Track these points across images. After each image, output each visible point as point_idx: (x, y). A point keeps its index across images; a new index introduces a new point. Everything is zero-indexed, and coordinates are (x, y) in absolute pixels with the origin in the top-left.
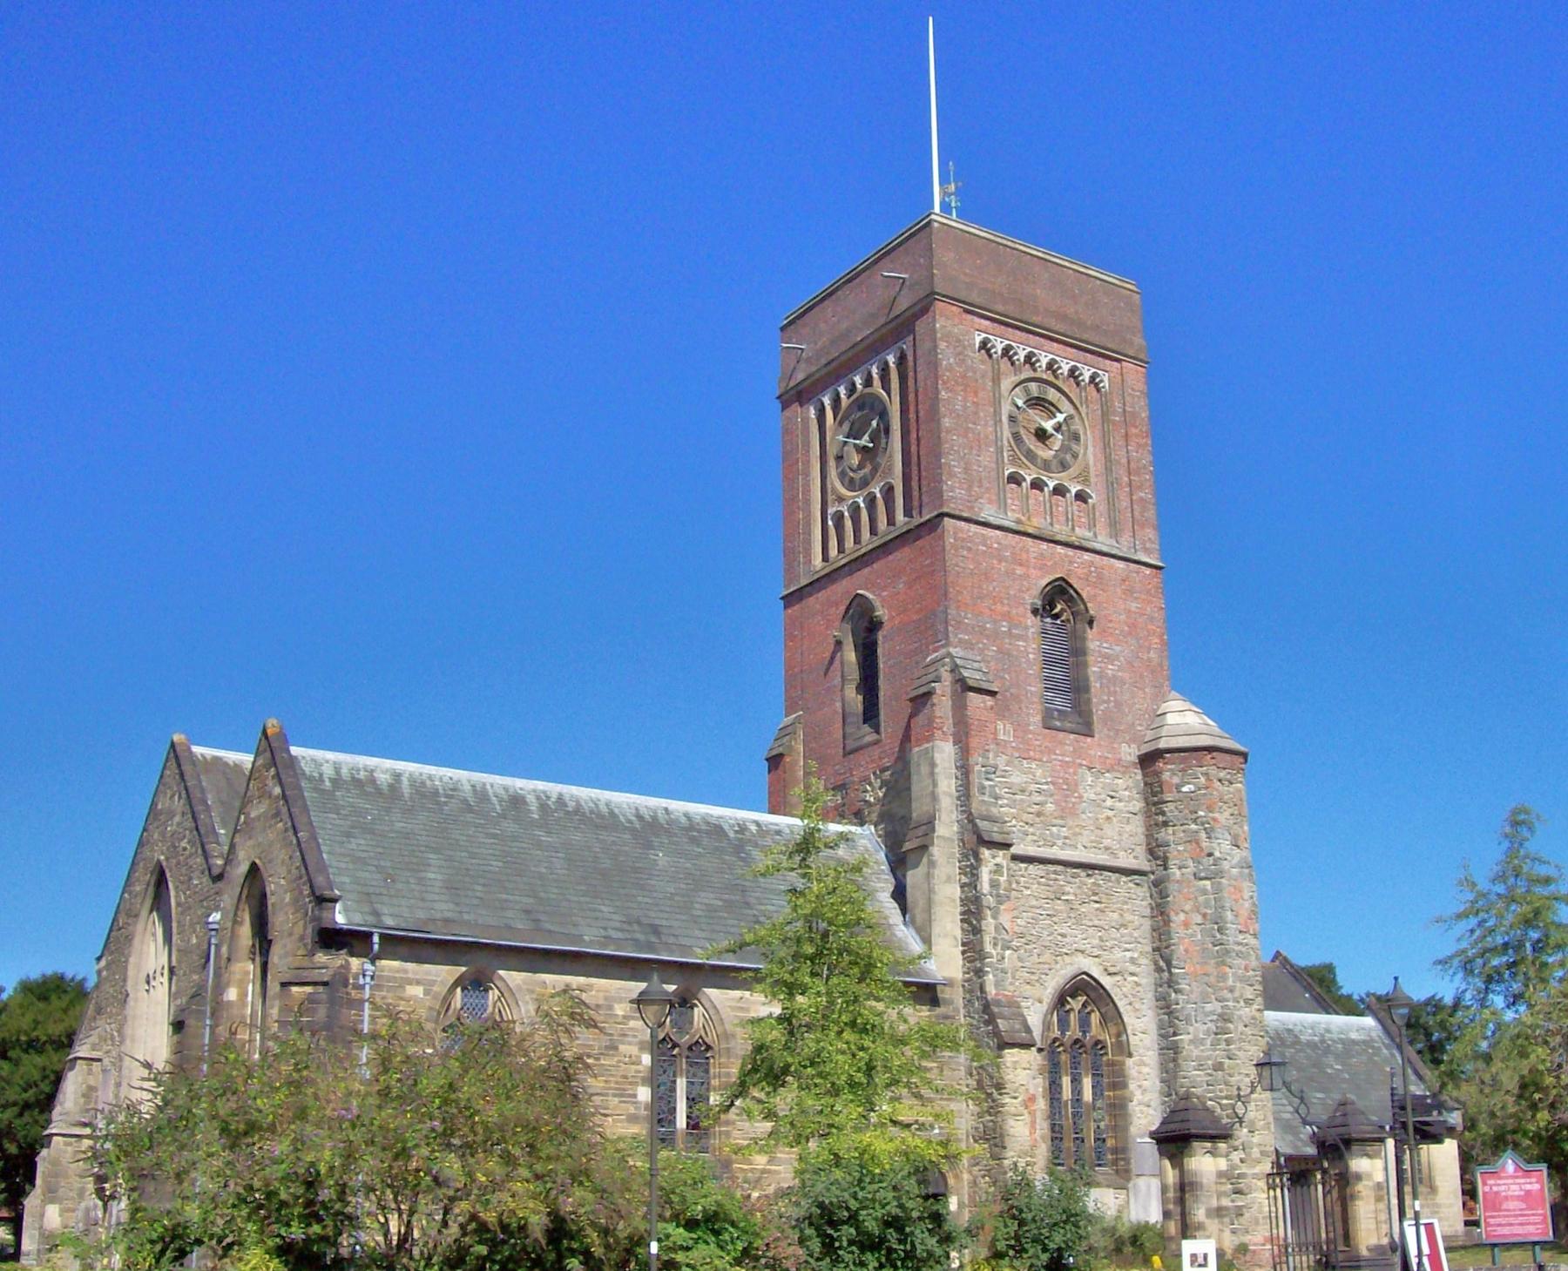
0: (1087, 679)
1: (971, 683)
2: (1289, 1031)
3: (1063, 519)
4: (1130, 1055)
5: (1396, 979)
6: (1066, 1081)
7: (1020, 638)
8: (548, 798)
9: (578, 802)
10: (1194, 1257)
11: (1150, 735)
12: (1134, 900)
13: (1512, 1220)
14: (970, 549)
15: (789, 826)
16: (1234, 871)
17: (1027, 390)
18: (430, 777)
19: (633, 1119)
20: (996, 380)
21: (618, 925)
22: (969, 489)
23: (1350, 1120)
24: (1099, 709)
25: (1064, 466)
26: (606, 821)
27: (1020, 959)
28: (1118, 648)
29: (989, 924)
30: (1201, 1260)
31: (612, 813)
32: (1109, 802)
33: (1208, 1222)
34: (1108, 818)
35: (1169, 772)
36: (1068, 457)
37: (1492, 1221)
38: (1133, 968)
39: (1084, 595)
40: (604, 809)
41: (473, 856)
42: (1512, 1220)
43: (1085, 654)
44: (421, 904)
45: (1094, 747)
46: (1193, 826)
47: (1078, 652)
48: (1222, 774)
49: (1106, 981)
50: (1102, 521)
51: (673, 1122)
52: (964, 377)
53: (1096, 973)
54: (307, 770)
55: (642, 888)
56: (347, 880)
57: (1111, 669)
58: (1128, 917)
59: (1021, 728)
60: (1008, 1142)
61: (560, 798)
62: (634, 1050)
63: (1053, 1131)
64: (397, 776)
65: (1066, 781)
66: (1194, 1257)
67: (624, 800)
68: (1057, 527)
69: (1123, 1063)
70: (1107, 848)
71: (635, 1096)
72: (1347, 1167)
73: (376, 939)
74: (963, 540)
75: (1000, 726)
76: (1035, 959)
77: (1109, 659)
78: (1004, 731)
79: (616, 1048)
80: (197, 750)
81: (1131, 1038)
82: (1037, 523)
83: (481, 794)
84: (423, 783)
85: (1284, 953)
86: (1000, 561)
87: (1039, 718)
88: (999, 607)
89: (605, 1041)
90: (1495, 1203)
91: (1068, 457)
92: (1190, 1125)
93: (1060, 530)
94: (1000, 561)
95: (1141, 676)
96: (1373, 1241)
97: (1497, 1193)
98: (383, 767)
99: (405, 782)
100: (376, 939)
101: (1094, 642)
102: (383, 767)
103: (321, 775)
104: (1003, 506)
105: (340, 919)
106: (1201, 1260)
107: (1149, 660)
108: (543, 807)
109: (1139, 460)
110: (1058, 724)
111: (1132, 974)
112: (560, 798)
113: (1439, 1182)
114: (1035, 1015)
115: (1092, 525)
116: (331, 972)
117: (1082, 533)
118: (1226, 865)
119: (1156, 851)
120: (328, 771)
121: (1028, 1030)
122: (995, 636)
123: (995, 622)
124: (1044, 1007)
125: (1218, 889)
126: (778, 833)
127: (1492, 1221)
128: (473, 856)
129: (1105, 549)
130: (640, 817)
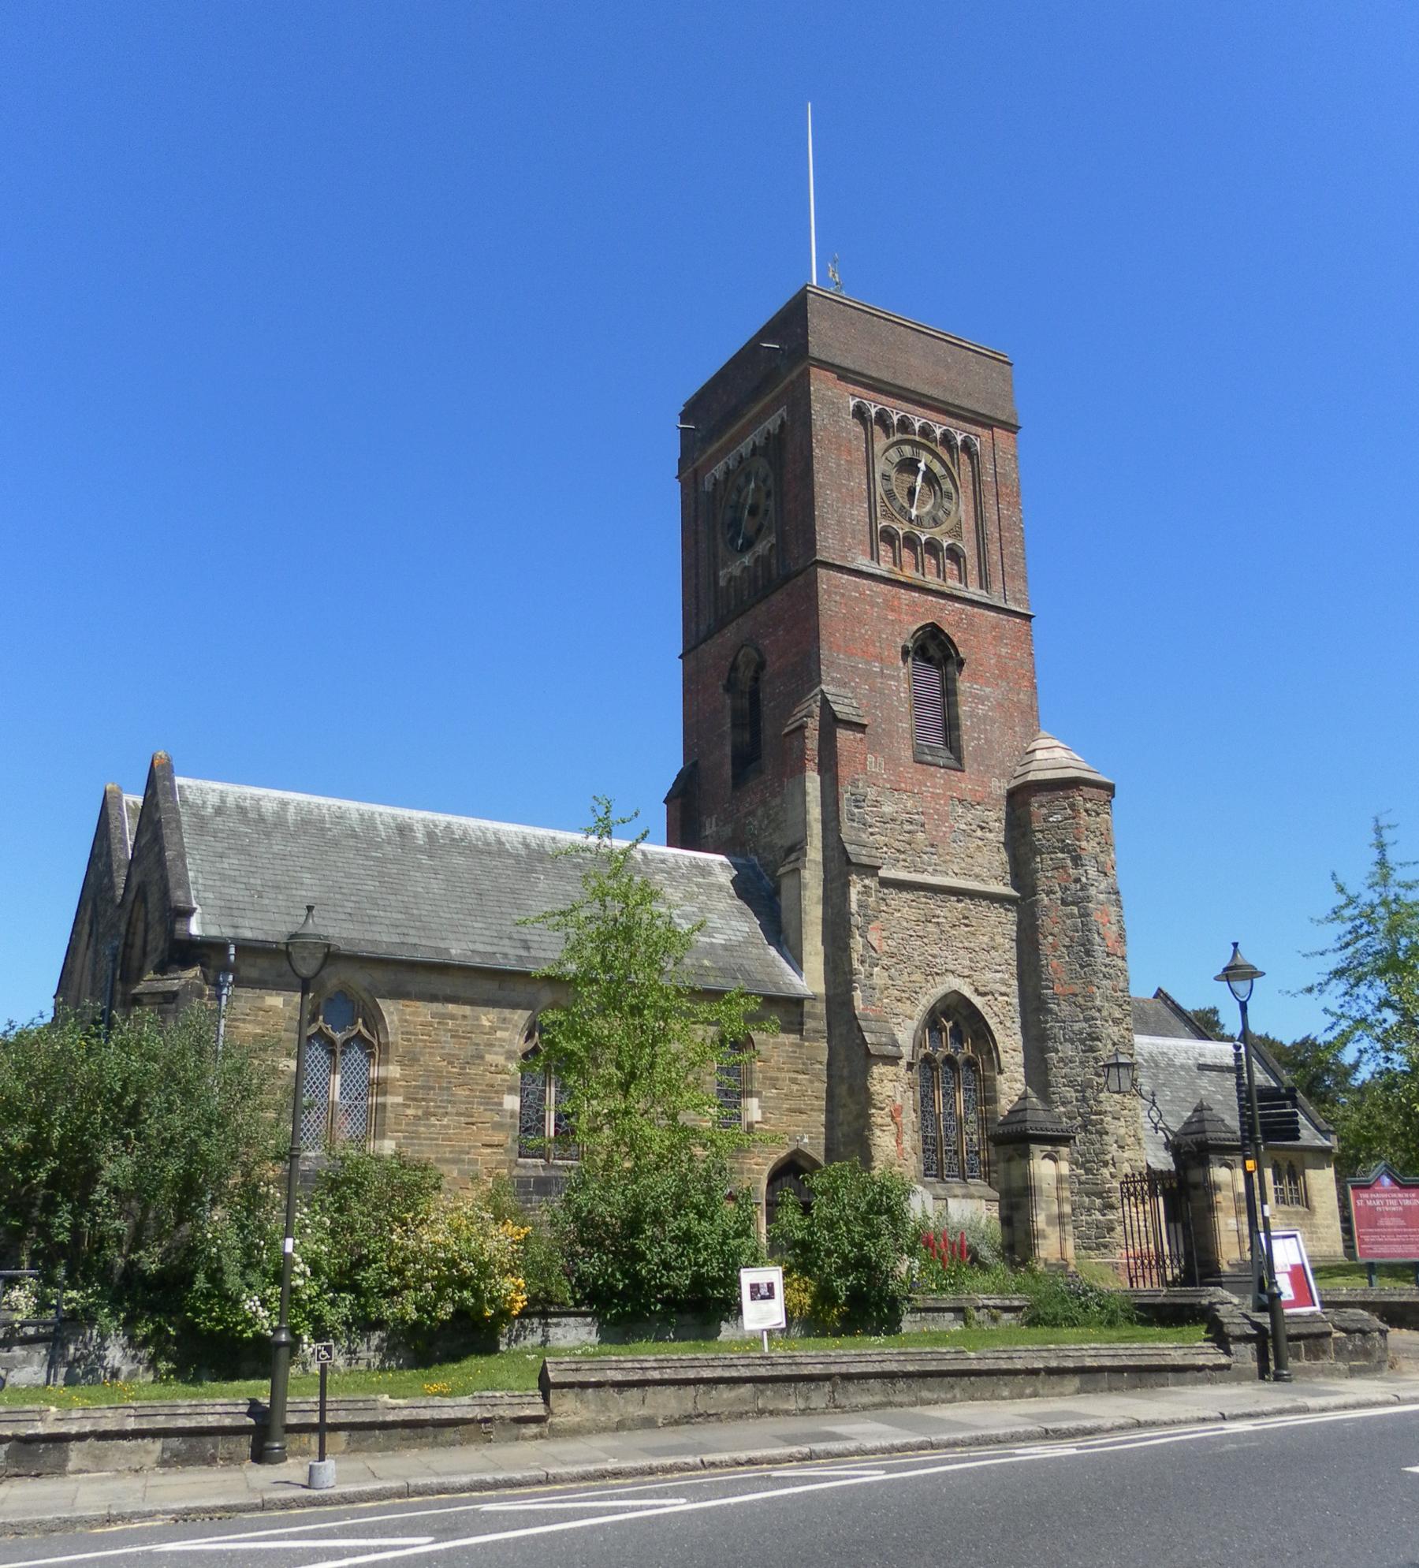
0: (957, 718)
1: (840, 716)
2: (1163, 1053)
3: (934, 571)
4: (1001, 1072)
5: (1235, 945)
6: (939, 1095)
7: (892, 677)
8: (436, 826)
9: (465, 832)
10: (755, 1288)
11: (1020, 770)
12: (1001, 926)
13: (1389, 1239)
14: (843, 595)
15: (674, 856)
16: (1102, 897)
17: (900, 452)
18: (318, 807)
19: (498, 1126)
20: (869, 442)
21: (490, 940)
22: (843, 539)
23: (1207, 1126)
24: (969, 745)
25: (936, 522)
26: (496, 850)
27: (891, 978)
28: (988, 690)
29: (857, 943)
31: (500, 842)
32: (979, 833)
33: (1049, 1230)
34: (979, 847)
35: (1038, 807)
36: (941, 513)
37: (1366, 1238)
38: (1004, 989)
39: (955, 640)
40: (491, 838)
41: (348, 875)
42: (1389, 1239)
43: (955, 694)
44: (287, 918)
45: (965, 783)
46: (1060, 855)
47: (949, 693)
48: (1089, 805)
49: (978, 1001)
50: (973, 574)
51: (541, 1131)
52: (838, 437)
53: (967, 992)
54: (191, 798)
56: (211, 895)
57: (981, 710)
58: (999, 940)
59: (892, 761)
60: (875, 1152)
61: (448, 827)
62: (501, 1060)
63: (925, 1143)
64: (284, 804)
65: (937, 811)
66: (755, 1288)
68: (928, 578)
69: (995, 1079)
70: (977, 876)
71: (501, 1104)
72: (1206, 1174)
73: (232, 950)
74: (836, 587)
75: (871, 758)
76: (906, 977)
77: (981, 700)
78: (874, 763)
79: (482, 1058)
81: (1003, 1056)
82: (909, 573)
83: (369, 823)
84: (310, 812)
85: (1165, 990)
86: (872, 607)
87: (909, 753)
88: (871, 649)
89: (470, 1050)
90: (1372, 1218)
91: (941, 513)
92: (1028, 1125)
93: (932, 581)
94: (872, 607)
95: (1011, 715)
96: (1234, 1256)
97: (1374, 1207)
98: (269, 797)
99: (291, 809)
100: (232, 950)
101: (963, 684)
103: (204, 803)
104: (874, 556)
106: (764, 1291)
107: (1019, 701)
108: (431, 835)
109: (1010, 517)
110: (929, 758)
111: (1002, 994)
112: (448, 827)
113: (1316, 1201)
114: (906, 1033)
115: (962, 577)
116: (183, 982)
117: (953, 584)
118: (1093, 891)
119: (1021, 871)
121: (895, 1044)
122: (868, 675)
123: (867, 662)
124: (914, 1024)
125: (1084, 914)
126: (663, 861)
127: (1366, 1238)
128: (348, 875)
129: (975, 598)
130: (527, 846)
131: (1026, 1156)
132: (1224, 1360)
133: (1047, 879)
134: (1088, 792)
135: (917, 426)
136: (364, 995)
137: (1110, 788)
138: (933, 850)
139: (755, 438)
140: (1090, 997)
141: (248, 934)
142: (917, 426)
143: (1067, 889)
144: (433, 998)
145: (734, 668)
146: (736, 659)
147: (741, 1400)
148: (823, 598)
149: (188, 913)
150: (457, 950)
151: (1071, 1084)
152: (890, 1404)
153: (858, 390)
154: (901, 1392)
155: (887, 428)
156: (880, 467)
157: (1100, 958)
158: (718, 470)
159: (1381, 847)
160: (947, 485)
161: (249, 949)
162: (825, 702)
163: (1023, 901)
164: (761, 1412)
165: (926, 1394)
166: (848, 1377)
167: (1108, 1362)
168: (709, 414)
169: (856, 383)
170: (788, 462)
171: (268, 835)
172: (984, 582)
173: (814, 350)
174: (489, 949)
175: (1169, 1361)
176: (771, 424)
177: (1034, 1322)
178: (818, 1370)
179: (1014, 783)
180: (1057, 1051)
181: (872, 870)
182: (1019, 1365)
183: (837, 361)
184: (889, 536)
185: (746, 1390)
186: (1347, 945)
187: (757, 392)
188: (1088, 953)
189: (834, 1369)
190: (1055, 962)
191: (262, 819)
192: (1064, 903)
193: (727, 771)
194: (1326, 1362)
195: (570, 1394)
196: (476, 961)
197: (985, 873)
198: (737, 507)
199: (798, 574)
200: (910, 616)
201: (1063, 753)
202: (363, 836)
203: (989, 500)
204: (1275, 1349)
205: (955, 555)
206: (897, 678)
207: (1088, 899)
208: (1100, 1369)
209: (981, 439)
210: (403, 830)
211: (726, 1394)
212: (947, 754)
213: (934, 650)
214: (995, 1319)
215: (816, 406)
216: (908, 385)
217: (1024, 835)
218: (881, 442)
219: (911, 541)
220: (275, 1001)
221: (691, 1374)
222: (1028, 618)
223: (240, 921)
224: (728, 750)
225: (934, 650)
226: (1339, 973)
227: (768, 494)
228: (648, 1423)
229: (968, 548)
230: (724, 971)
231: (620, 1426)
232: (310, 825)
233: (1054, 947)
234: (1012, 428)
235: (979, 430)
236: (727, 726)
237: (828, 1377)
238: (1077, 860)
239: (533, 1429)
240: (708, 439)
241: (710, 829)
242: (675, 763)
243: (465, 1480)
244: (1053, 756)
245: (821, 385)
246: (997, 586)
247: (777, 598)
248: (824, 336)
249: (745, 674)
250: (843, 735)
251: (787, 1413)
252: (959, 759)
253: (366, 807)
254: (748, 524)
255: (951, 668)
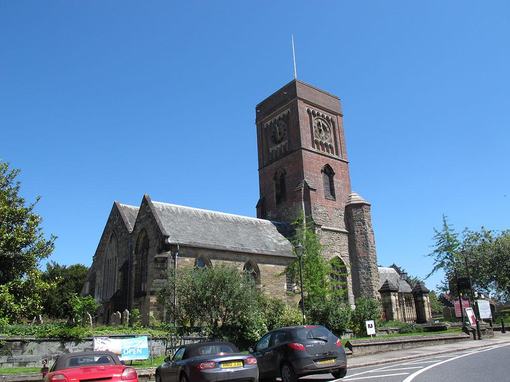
12: (345, 239)
26: (226, 221)
30: (371, 326)
41: (197, 227)
45: (336, 204)
55: (237, 235)
67: (229, 215)
68: (326, 152)
80: (121, 205)
82: (321, 151)
98: (173, 206)
101: (335, 179)
102: (173, 206)
105: (169, 241)
106: (371, 326)
115: (333, 153)
120: (161, 207)
125: (366, 237)
126: (264, 223)
131: (390, 295)
132: (469, 336)
133: (357, 228)
134: (366, 206)
135: (321, 114)
136: (207, 258)
137: (370, 205)
138: (455, 236)
139: (281, 115)
140: (368, 257)
141: (181, 243)
142: (321, 114)
143: (362, 231)
144: (223, 259)
145: (276, 173)
146: (276, 172)
147: (386, 348)
148: (303, 157)
149: (168, 237)
150: (228, 247)
151: (364, 279)
152: (413, 348)
153: (308, 105)
154: (414, 345)
155: (315, 116)
156: (314, 124)
157: (370, 248)
158: (268, 123)
159: (445, 221)
160: (328, 129)
161: (182, 246)
162: (306, 184)
163: (350, 234)
164: (390, 351)
165: (419, 345)
166: (405, 342)
167: (448, 337)
168: (264, 109)
169: (308, 104)
170: (291, 123)
171: (176, 216)
172: (337, 154)
173: (298, 95)
174: (235, 246)
175: (459, 336)
176: (285, 112)
177: (400, 333)
178: (399, 341)
179: (347, 204)
180: (361, 271)
181: (320, 226)
182: (434, 338)
183: (303, 98)
184: (316, 142)
185: (387, 346)
186: (438, 245)
187: (281, 104)
188: (368, 246)
189: (402, 341)
190: (360, 249)
191: (173, 212)
192: (361, 234)
193: (275, 200)
194: (486, 336)
195: (356, 348)
196: (233, 249)
197: (341, 227)
198: (275, 132)
199: (296, 151)
200: (322, 162)
201: (358, 197)
202: (196, 217)
203: (337, 133)
204: (478, 333)
205: (331, 147)
206: (320, 177)
207: (367, 233)
208: (449, 339)
209: (335, 118)
210: (205, 215)
211: (383, 347)
212: (332, 196)
213: (328, 171)
214: (393, 332)
215: (299, 109)
216: (319, 105)
217: (350, 217)
218: (313, 118)
219: (321, 143)
220: (187, 260)
221: (377, 343)
222: (347, 163)
223: (179, 239)
224: (275, 194)
225: (328, 171)
226: (437, 251)
227: (285, 130)
228: (370, 354)
229: (333, 145)
230: (286, 251)
231: (366, 355)
232: (184, 214)
233: (359, 245)
234: (341, 116)
235: (334, 116)
236: (274, 188)
237: (401, 343)
238: (364, 224)
239: (350, 356)
240: (266, 115)
241: (269, 214)
242: (257, 198)
243: (363, 364)
244: (356, 198)
245: (300, 104)
246: (340, 155)
247: (289, 156)
248: (300, 92)
249: (279, 175)
250: (311, 192)
251: (395, 350)
252: (335, 198)
253: (204, 211)
254: (279, 137)
255: (332, 175)
